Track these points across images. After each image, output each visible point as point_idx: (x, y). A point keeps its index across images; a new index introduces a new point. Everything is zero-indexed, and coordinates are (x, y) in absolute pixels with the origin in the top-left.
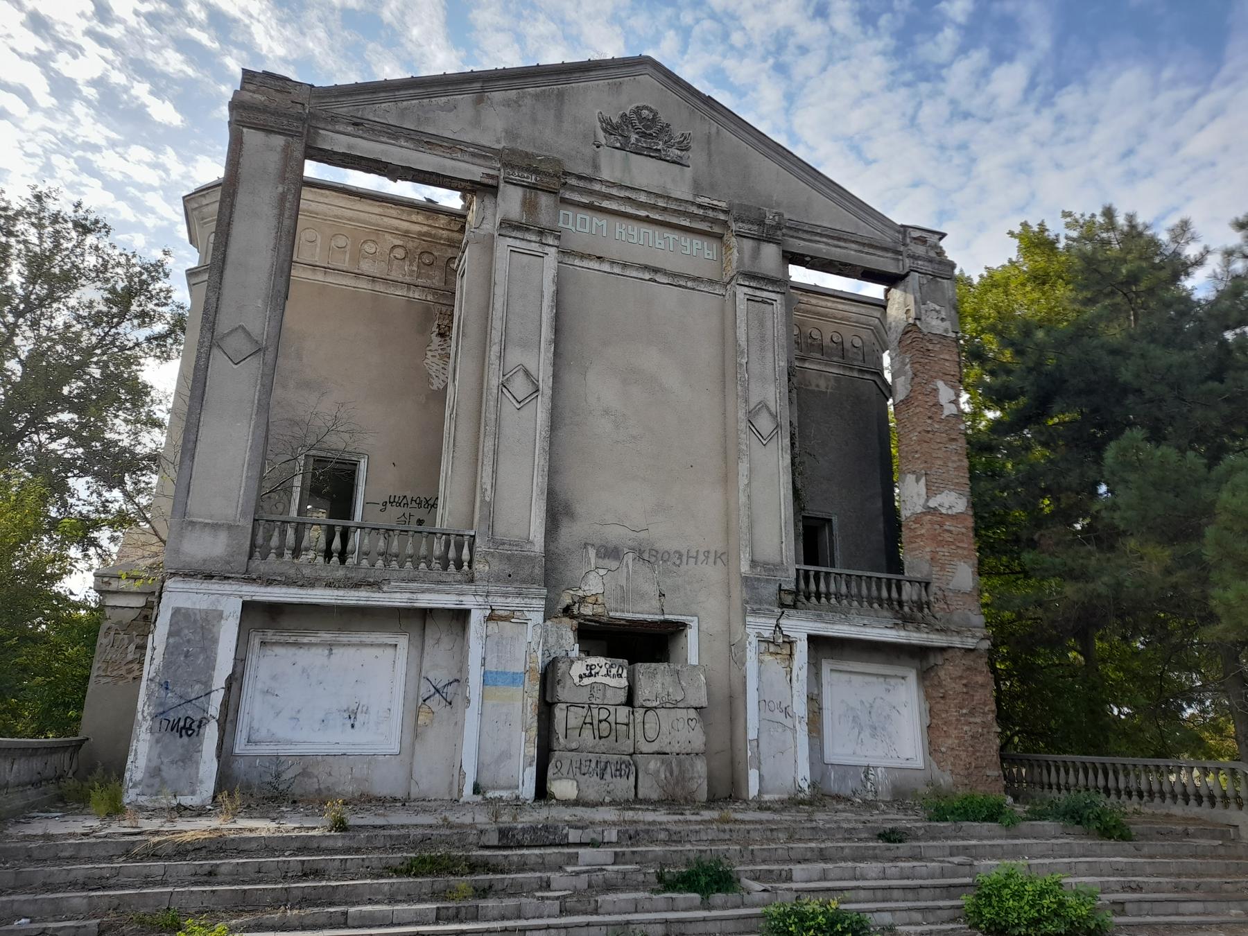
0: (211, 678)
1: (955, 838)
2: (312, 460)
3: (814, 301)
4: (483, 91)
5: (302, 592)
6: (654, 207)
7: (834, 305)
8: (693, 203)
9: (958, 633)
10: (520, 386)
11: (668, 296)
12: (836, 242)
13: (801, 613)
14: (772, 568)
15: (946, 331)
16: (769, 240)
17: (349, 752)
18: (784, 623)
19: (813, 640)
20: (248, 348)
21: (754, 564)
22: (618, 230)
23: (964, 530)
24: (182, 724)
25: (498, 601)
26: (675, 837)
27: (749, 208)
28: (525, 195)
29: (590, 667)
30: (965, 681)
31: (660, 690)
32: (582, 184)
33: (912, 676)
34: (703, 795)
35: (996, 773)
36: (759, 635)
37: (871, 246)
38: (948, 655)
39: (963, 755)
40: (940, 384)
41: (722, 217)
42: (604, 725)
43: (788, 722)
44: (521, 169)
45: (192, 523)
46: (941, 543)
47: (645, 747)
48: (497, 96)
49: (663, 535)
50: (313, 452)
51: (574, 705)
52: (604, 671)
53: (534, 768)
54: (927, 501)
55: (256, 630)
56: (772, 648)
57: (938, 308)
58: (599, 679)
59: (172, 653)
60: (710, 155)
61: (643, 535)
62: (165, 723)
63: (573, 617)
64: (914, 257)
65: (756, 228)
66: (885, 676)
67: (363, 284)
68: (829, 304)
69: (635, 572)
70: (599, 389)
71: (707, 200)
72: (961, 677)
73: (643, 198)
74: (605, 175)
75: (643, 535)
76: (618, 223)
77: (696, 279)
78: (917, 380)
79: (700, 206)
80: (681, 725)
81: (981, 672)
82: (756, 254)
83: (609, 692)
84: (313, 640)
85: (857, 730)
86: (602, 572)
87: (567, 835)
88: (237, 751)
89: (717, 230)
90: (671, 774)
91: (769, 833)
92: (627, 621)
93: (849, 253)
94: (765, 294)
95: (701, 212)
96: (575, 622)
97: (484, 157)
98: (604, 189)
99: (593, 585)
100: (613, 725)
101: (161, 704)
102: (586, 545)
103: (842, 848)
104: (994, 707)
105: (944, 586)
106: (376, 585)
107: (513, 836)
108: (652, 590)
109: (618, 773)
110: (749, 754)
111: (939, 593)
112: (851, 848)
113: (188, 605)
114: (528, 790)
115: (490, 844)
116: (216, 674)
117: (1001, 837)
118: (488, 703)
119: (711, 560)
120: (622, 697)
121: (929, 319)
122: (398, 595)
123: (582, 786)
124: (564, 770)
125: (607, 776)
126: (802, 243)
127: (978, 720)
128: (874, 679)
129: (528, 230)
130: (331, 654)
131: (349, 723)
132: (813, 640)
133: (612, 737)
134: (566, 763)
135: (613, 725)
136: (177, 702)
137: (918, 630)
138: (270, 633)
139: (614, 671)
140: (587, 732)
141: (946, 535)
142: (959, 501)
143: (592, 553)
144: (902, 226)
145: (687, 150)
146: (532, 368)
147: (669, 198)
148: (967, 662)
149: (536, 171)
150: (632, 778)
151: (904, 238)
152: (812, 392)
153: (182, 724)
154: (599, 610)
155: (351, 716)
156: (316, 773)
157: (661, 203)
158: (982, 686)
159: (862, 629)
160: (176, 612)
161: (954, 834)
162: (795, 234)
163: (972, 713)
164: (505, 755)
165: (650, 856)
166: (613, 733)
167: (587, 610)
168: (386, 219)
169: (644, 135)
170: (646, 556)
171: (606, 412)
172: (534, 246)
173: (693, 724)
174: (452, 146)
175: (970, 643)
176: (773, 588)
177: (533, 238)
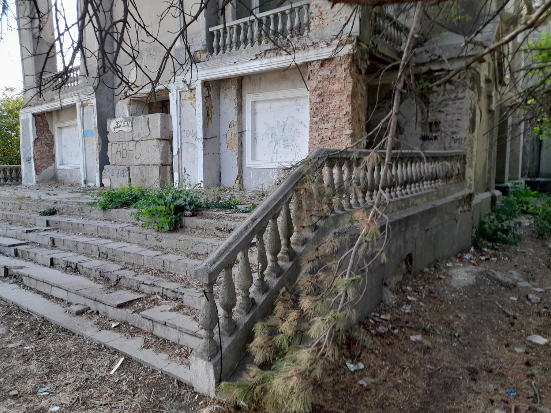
5: (40, 107)
42: (125, 151)
58: (121, 129)
85: (274, 143)
125: (119, 177)
128: (287, 103)
133: (127, 158)
134: (107, 170)
159: (235, 66)
173: (155, 148)
175: (326, 52)
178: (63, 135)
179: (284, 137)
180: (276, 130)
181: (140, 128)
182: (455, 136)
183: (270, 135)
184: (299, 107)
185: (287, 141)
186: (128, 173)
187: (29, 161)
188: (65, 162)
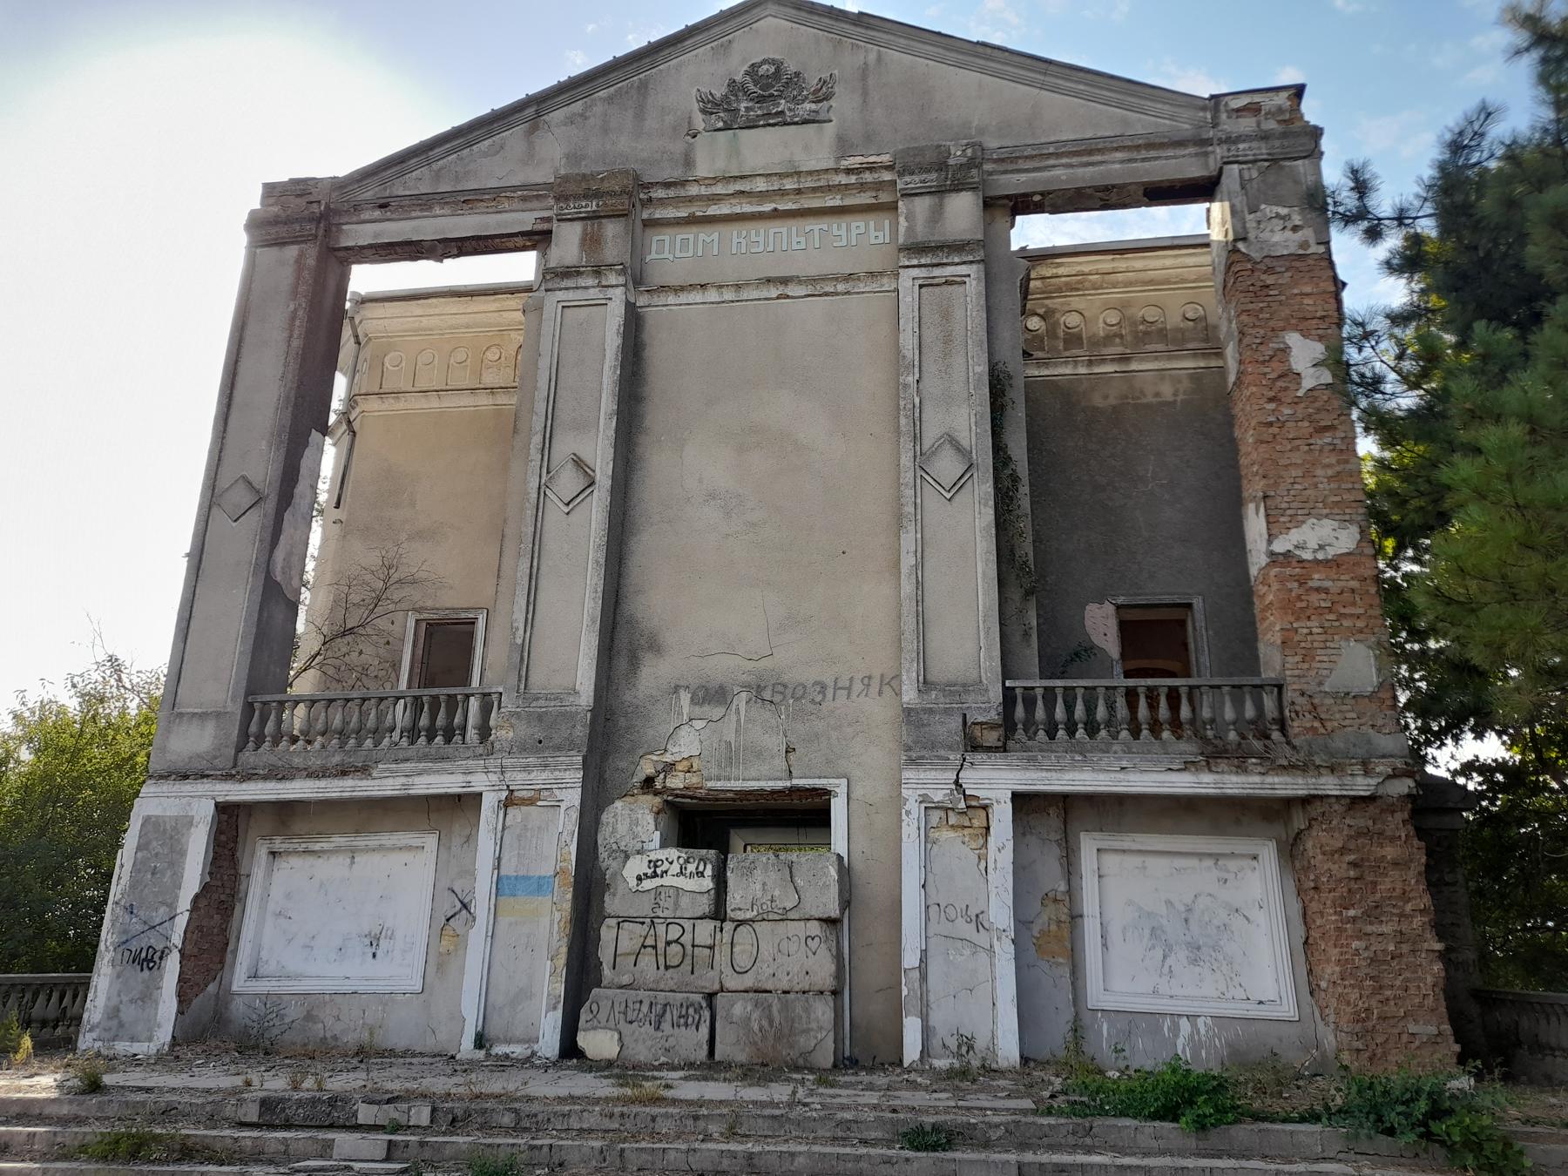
0: (176, 897)
1: (1074, 1148)
2: (424, 625)
3: (1139, 264)
4: (538, 115)
5: (280, 785)
6: (782, 193)
7: (1179, 261)
8: (837, 171)
9: (1332, 770)
10: (568, 482)
11: (809, 312)
12: (1085, 159)
13: (1013, 757)
14: (959, 689)
15: (1304, 245)
16: (957, 188)
17: (361, 989)
18: (968, 777)
19: (1019, 799)
20: (247, 499)
21: (926, 685)
22: (735, 240)
23: (1354, 584)
24: (143, 955)
25: (517, 779)
26: (526, 1123)
27: (920, 151)
28: (585, 230)
29: (654, 864)
30: (1352, 857)
31: (759, 894)
32: (672, 193)
33: (1268, 852)
34: (826, 1058)
35: (1433, 1030)
36: (924, 799)
37: (1150, 146)
38: (1317, 809)
39: (1354, 995)
40: (1293, 339)
41: (887, 176)
42: (675, 948)
43: (982, 939)
44: (576, 197)
45: (181, 715)
46: (1304, 614)
47: (732, 982)
48: (557, 116)
49: (795, 660)
50: (425, 616)
51: (628, 919)
52: (675, 868)
53: (559, 1013)
54: (1270, 542)
55: (263, 837)
56: (953, 820)
57: (1283, 211)
58: (667, 881)
59: (139, 871)
60: (865, 94)
61: (764, 663)
62: (127, 954)
63: (656, 793)
64: (1230, 140)
65: (934, 176)
66: (1216, 857)
67: (484, 400)
68: (1168, 262)
69: (748, 721)
70: (691, 467)
71: (859, 159)
72: (1343, 851)
73: (761, 185)
74: (702, 171)
75: (764, 663)
76: (735, 233)
77: (849, 277)
78: (1246, 341)
79: (849, 171)
80: (793, 948)
81: (1393, 839)
82: (937, 215)
83: (685, 901)
84: (326, 846)
85: (1159, 953)
86: (699, 724)
87: (355, 1114)
88: (235, 988)
89: (885, 197)
90: (771, 1022)
91: (690, 1122)
92: (736, 792)
93: (1115, 169)
94: (949, 271)
95: (853, 179)
96: (658, 800)
97: (537, 197)
98: (704, 191)
99: (686, 745)
100: (689, 948)
101: (125, 932)
102: (676, 689)
103: (793, 1155)
104: (1426, 901)
105: (1311, 688)
106: (364, 771)
107: (283, 1110)
108: (775, 743)
109: (683, 1021)
110: (905, 992)
111: (1300, 700)
112: (810, 1154)
113: (158, 812)
114: (549, 1044)
115: (248, 1119)
116: (182, 893)
117: (1182, 1153)
118: (504, 921)
119: (874, 689)
120: (705, 905)
121: (1265, 235)
122: (390, 781)
123: (626, 1040)
124: (602, 1016)
125: (666, 1026)
126: (1023, 177)
127: (1386, 929)
128: (1193, 862)
129: (579, 273)
130: (353, 863)
131: (370, 951)
132: (1019, 799)
133: (686, 967)
134: (605, 1006)
135: (689, 948)
136: (140, 928)
137: (1242, 769)
138: (278, 840)
139: (691, 868)
140: (647, 960)
141: (1314, 598)
142: (1343, 534)
143: (685, 698)
144: (1213, 97)
145: (827, 98)
146: (586, 456)
147: (799, 173)
148: (1360, 821)
149: (597, 195)
150: (704, 1030)
151: (1215, 117)
152: (1148, 406)
153: (143, 955)
154: (693, 780)
155: (374, 941)
156: (322, 1016)
157: (789, 184)
158: (1396, 864)
159: (1121, 776)
160: (147, 820)
161: (1071, 1140)
162: (1010, 167)
163: (1374, 913)
164: (525, 994)
165: (448, 1152)
166: (688, 960)
167: (676, 782)
168: (505, 314)
169: (761, 100)
170: (767, 695)
171: (712, 496)
172: (593, 293)
173: (814, 944)
174: (493, 197)
175: (1362, 785)
176: (955, 723)
177: (590, 282)
178: (276, 875)
179: (1188, 938)
180: (1164, 922)
181: (758, 886)
182: (1453, 956)
183: (1147, 932)
184: (1226, 876)
185: (1199, 948)
186: (706, 1014)
187: (148, 961)
188: (260, 972)
